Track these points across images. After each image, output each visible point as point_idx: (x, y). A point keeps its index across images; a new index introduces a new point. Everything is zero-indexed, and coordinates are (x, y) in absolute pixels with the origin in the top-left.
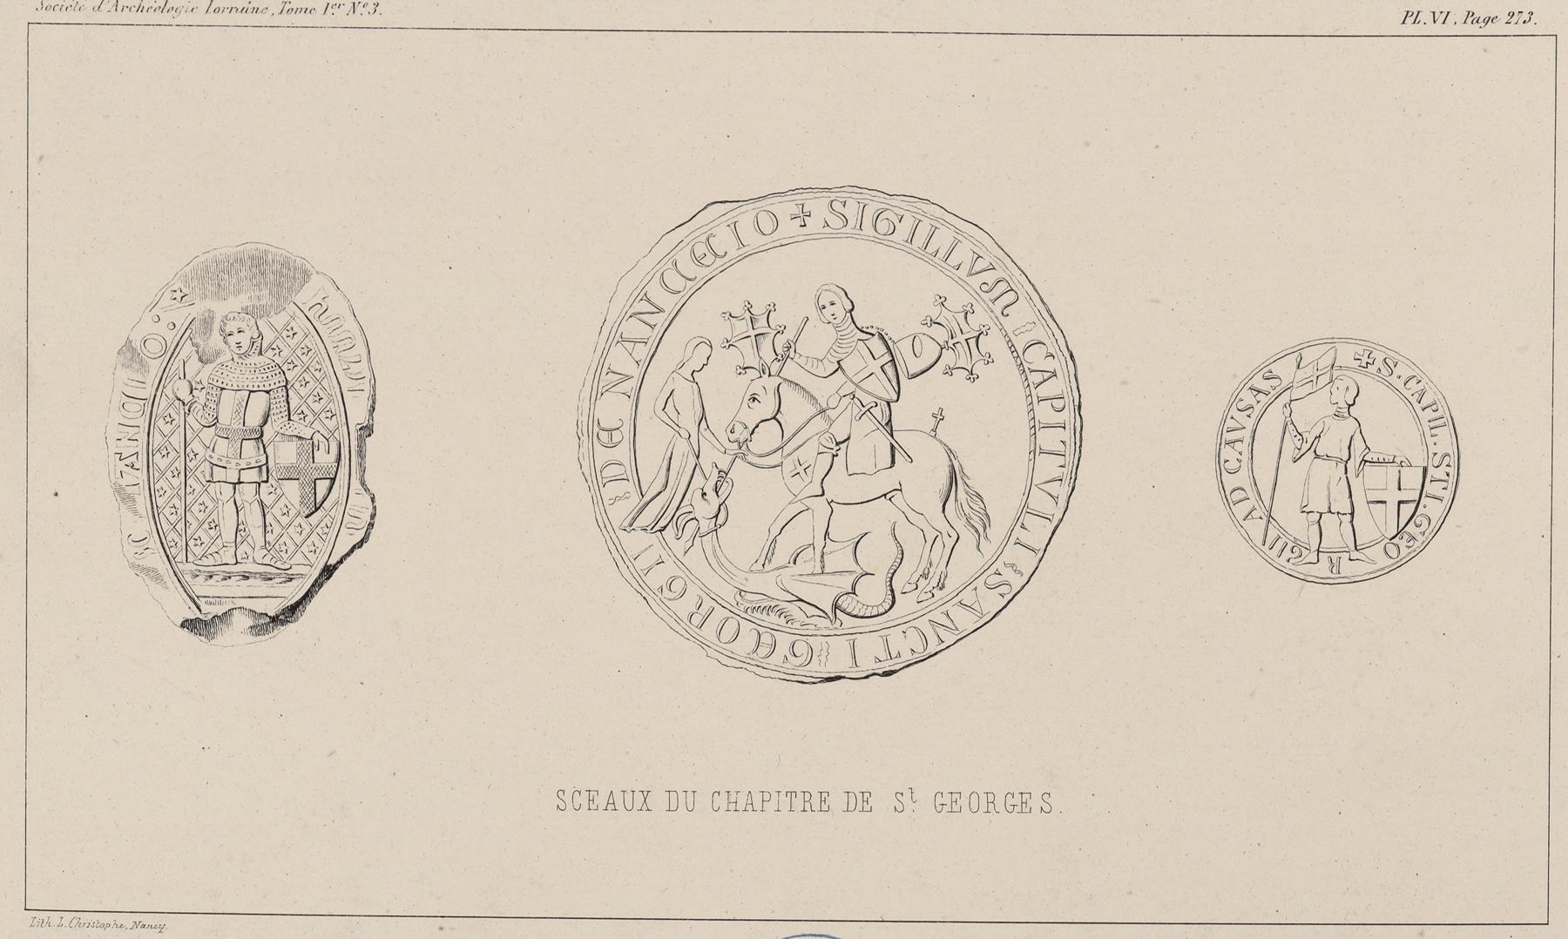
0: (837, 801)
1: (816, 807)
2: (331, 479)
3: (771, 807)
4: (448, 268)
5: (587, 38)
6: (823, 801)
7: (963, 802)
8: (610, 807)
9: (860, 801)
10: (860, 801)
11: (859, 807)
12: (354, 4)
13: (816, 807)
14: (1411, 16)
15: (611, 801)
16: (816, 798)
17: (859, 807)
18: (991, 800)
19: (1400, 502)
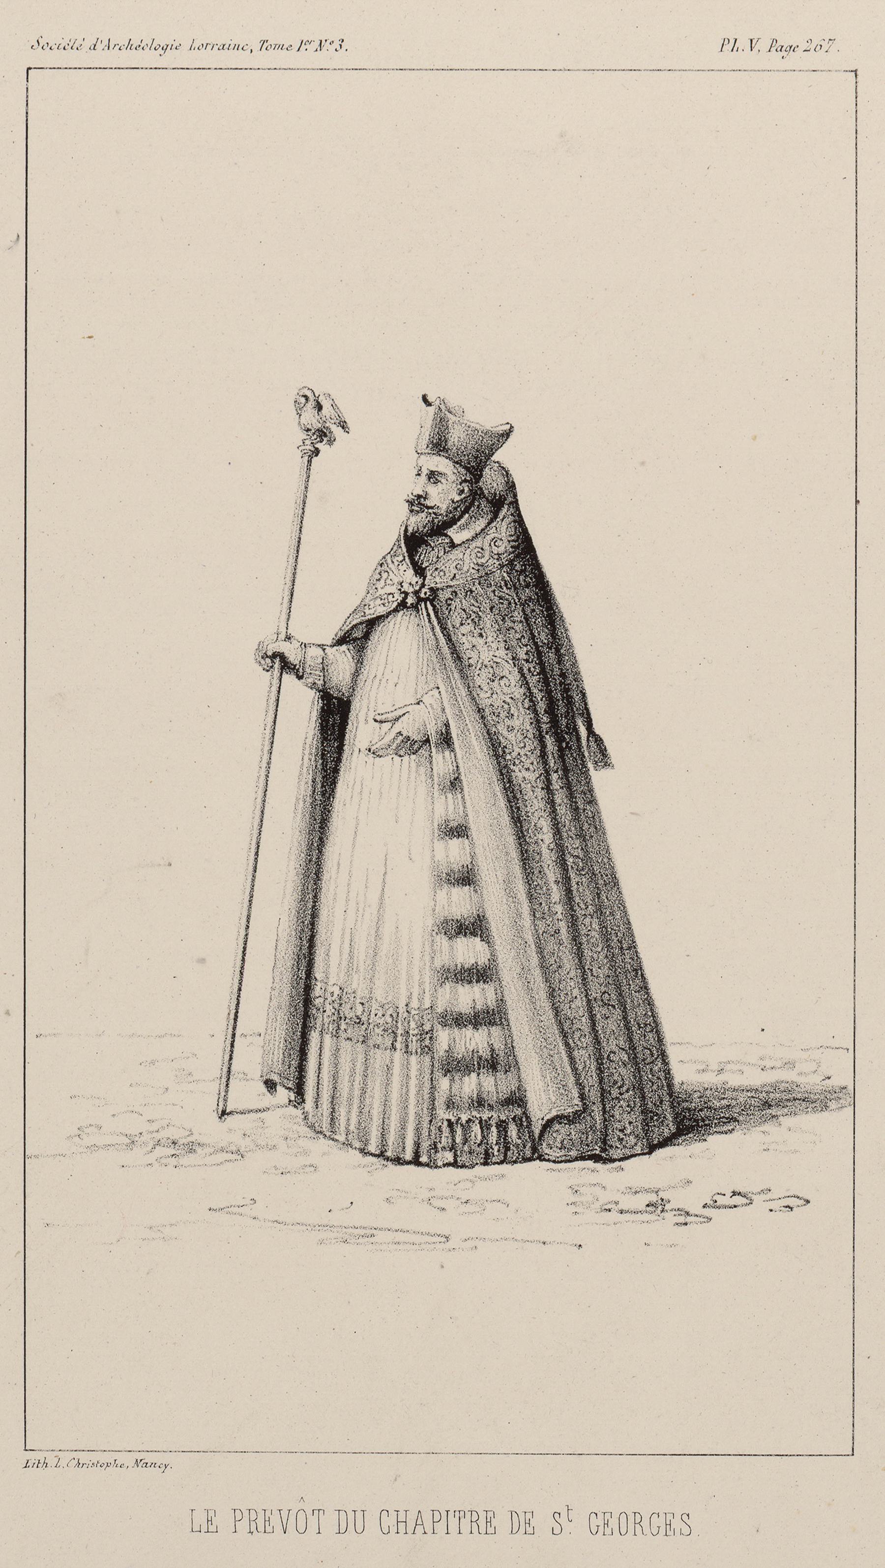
0: (502, 1522)
1: (261, 1528)
2: (456, 1161)
3: (441, 1527)
4: (231, 464)
5: (788, 1190)
6: (488, 1522)
7: (614, 1523)
8: (420, 1529)
9: (522, 1523)
10: (522, 1523)
11: (522, 1530)
12: (321, 41)
13: (261, 1528)
14: (730, 44)
15: (419, 1522)
16: (483, 1515)
17: (522, 1530)
18: (638, 1520)
19: (29, 69)
